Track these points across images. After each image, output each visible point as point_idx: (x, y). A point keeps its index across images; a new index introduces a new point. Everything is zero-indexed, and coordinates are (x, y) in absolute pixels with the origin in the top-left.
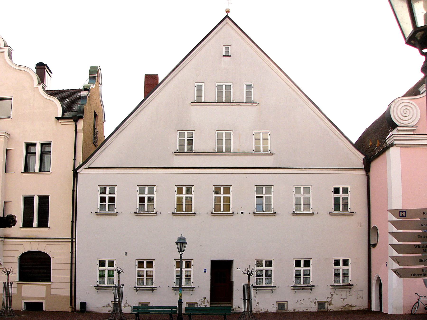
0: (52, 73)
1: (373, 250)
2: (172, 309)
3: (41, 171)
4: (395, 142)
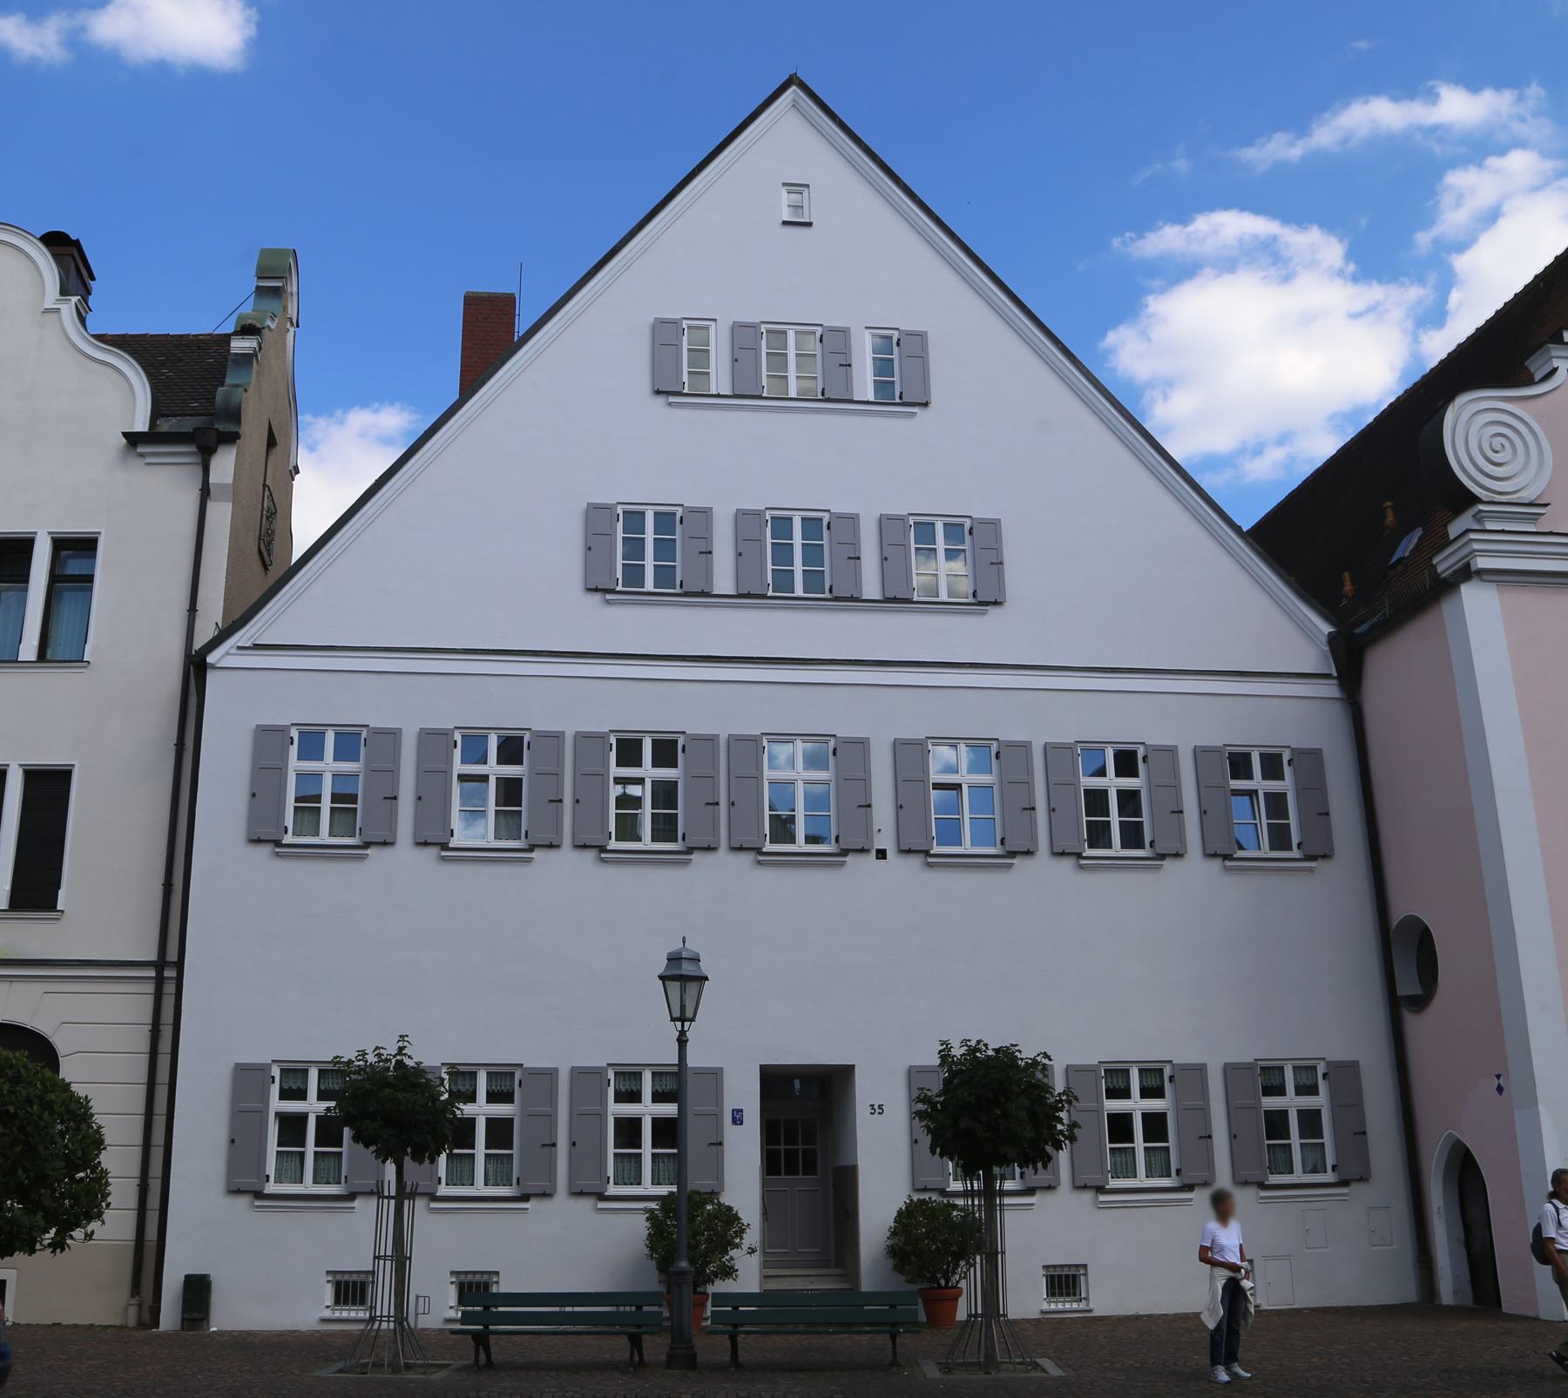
0: (93, 278)
1: (1416, 1025)
2: (735, 1308)
3: (42, 656)
4: (1482, 563)
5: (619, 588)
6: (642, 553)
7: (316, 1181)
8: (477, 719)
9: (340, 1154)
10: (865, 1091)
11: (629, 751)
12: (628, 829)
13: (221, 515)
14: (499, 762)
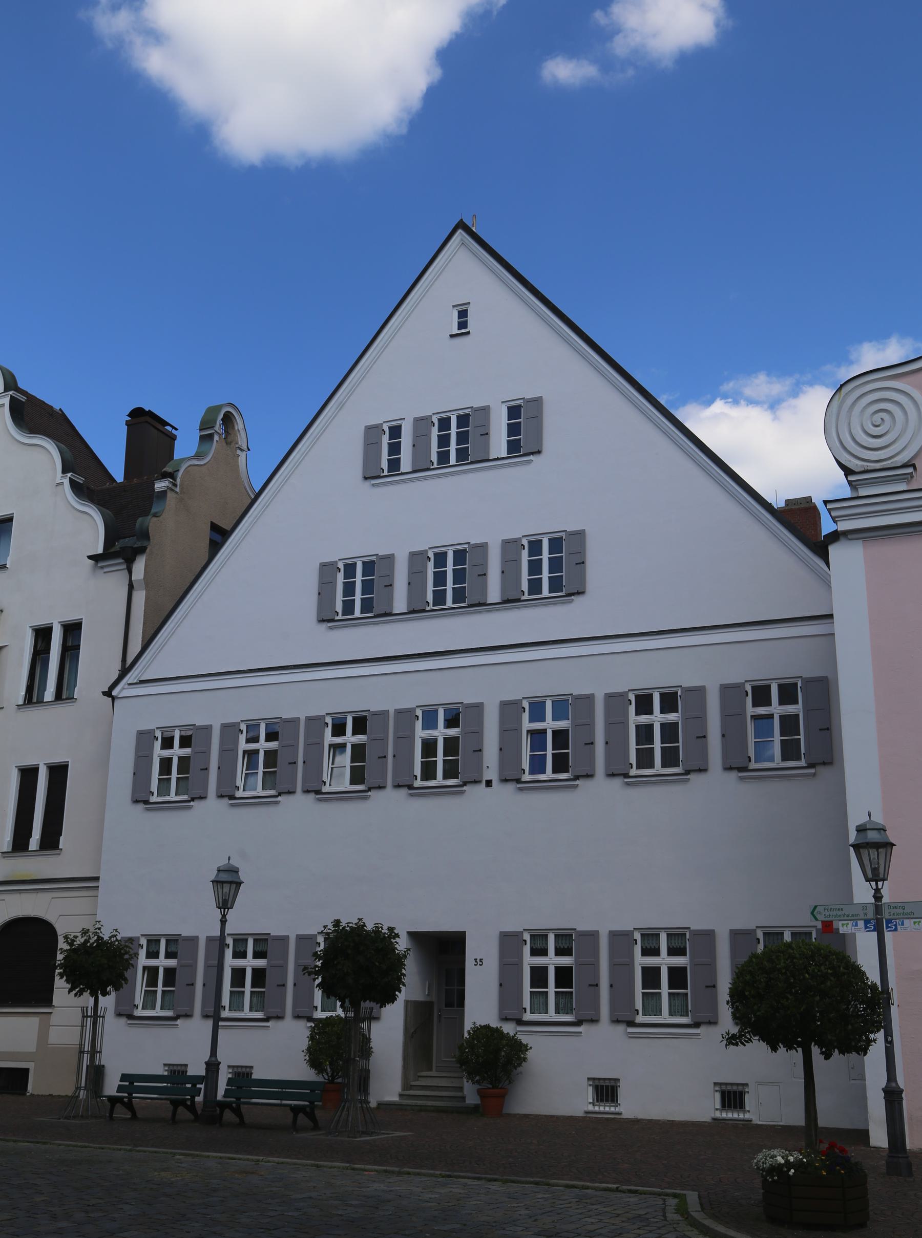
0: (176, 429)
2: (131, 1083)
6: (357, 590)
7: (557, 1012)
9: (687, 994)
10: (472, 951)
11: (644, 704)
12: (645, 759)
13: (140, 597)
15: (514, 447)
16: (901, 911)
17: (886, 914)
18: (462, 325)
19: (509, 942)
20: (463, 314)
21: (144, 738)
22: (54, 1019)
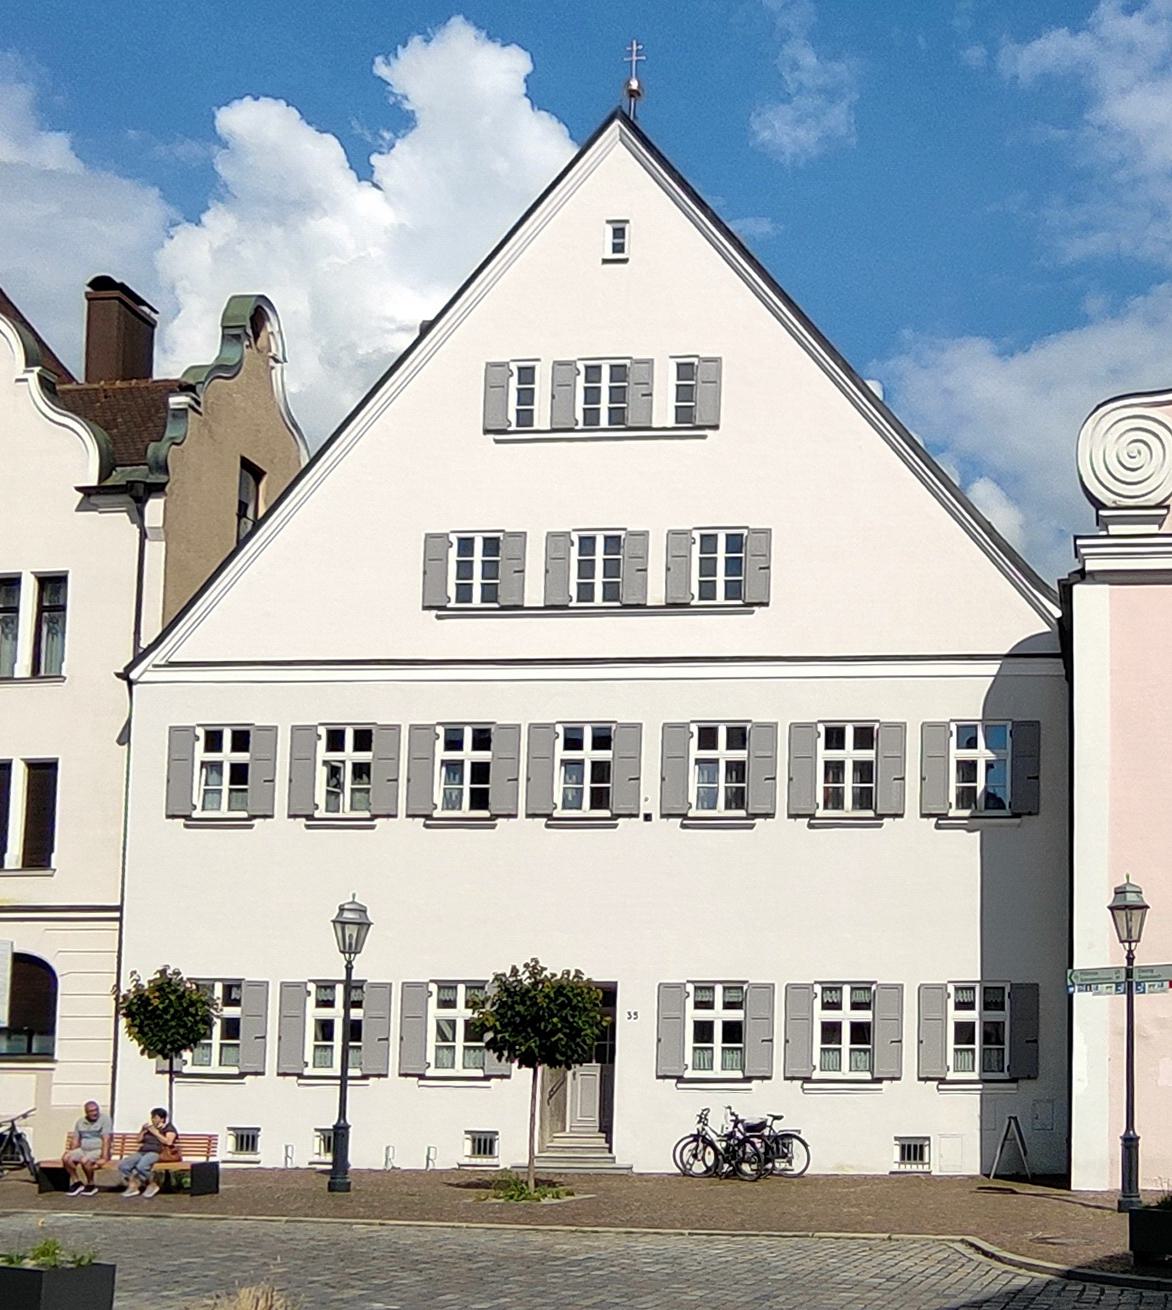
5: (574, 604)
6: (476, 573)
8: (214, 719)
11: (835, 738)
13: (156, 551)
14: (855, 748)
15: (684, 415)
16: (1149, 974)
17: (1136, 978)
18: (618, 248)
19: (669, 993)
20: (619, 233)
21: (179, 736)
22: (56, 1077)
